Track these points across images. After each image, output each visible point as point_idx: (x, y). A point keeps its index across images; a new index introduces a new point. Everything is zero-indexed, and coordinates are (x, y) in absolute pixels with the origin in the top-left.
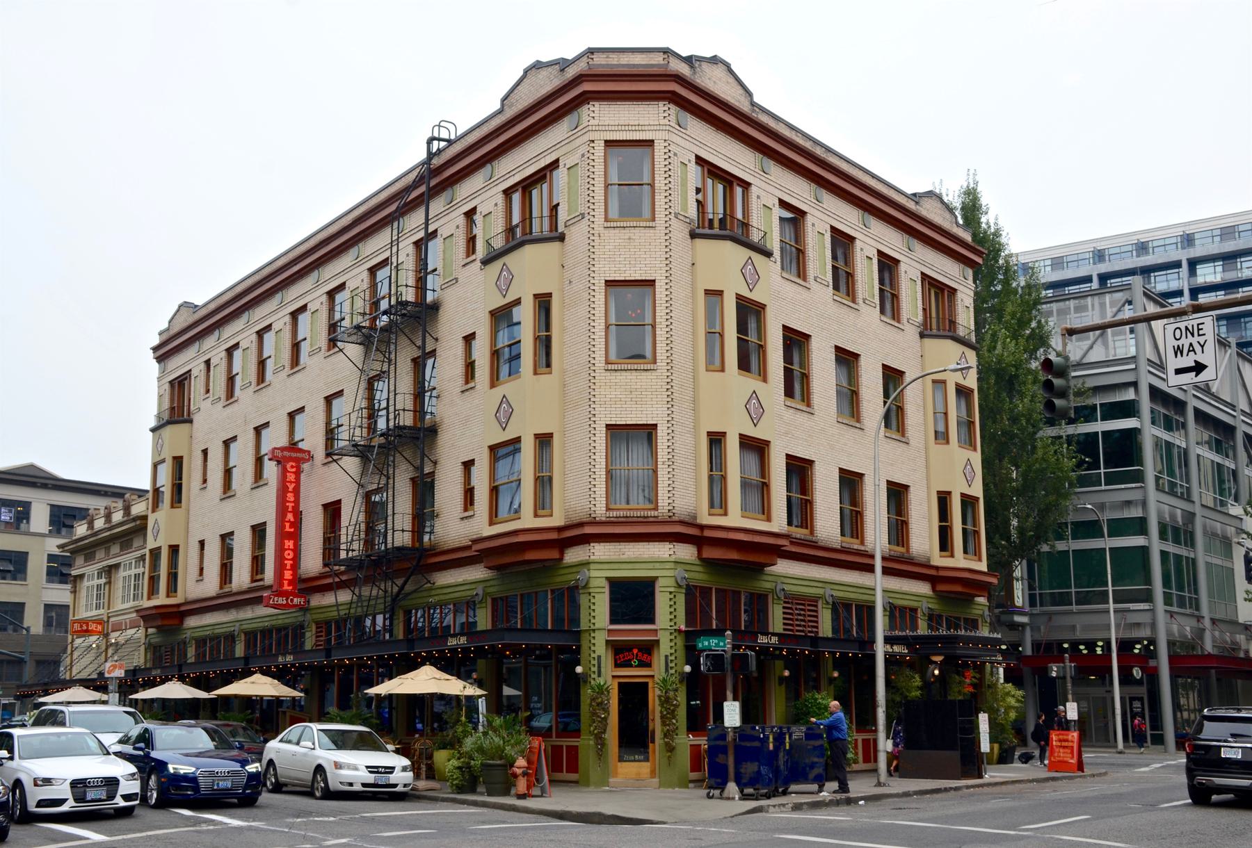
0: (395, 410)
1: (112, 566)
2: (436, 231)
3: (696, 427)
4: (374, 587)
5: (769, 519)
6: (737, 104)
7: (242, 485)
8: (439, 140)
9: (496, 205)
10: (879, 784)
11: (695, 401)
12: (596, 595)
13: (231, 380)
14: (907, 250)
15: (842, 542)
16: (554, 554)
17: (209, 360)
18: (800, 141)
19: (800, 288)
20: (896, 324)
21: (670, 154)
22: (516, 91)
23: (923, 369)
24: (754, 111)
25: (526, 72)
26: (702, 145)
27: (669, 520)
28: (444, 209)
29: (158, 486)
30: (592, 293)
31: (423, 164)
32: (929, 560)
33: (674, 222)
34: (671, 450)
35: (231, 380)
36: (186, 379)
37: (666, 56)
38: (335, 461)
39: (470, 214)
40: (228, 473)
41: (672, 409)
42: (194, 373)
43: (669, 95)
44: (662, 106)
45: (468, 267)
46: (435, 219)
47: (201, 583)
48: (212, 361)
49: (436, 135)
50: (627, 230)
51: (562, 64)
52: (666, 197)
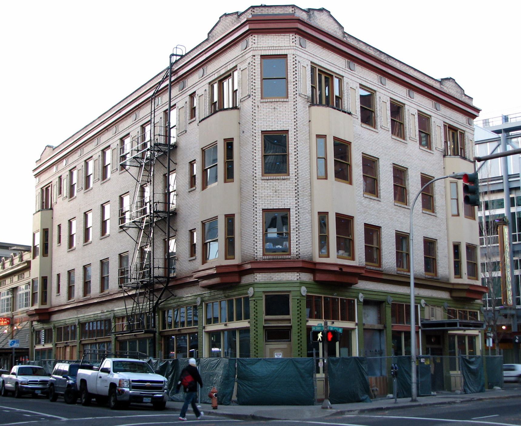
0: (154, 203)
1: (14, 288)
2: (175, 105)
3: (312, 210)
4: (145, 299)
5: (353, 259)
6: (335, 33)
7: (78, 244)
8: (176, 55)
9: (206, 90)
10: (413, 401)
11: (311, 195)
12: (258, 301)
13: (72, 187)
14: (435, 110)
15: (398, 270)
16: (235, 279)
17: (61, 176)
18: (372, 52)
19: (373, 132)
20: (429, 151)
21: (296, 62)
22: (215, 29)
23: (445, 173)
24: (344, 37)
25: (220, 18)
26: (314, 56)
27: (297, 260)
28: (179, 93)
29: (36, 245)
30: (254, 138)
31: (168, 69)
32: (448, 279)
33: (299, 98)
34: (298, 222)
35: (72, 187)
36: (49, 186)
37: (294, 9)
38: (124, 230)
39: (192, 96)
40: (71, 237)
41: (298, 200)
42: (54, 183)
43: (295, 30)
44: (291, 36)
45: (191, 124)
46: (174, 98)
47: (58, 297)
48: (62, 177)
49: (175, 53)
50: (273, 104)
51: (239, 15)
52: (294, 85)
